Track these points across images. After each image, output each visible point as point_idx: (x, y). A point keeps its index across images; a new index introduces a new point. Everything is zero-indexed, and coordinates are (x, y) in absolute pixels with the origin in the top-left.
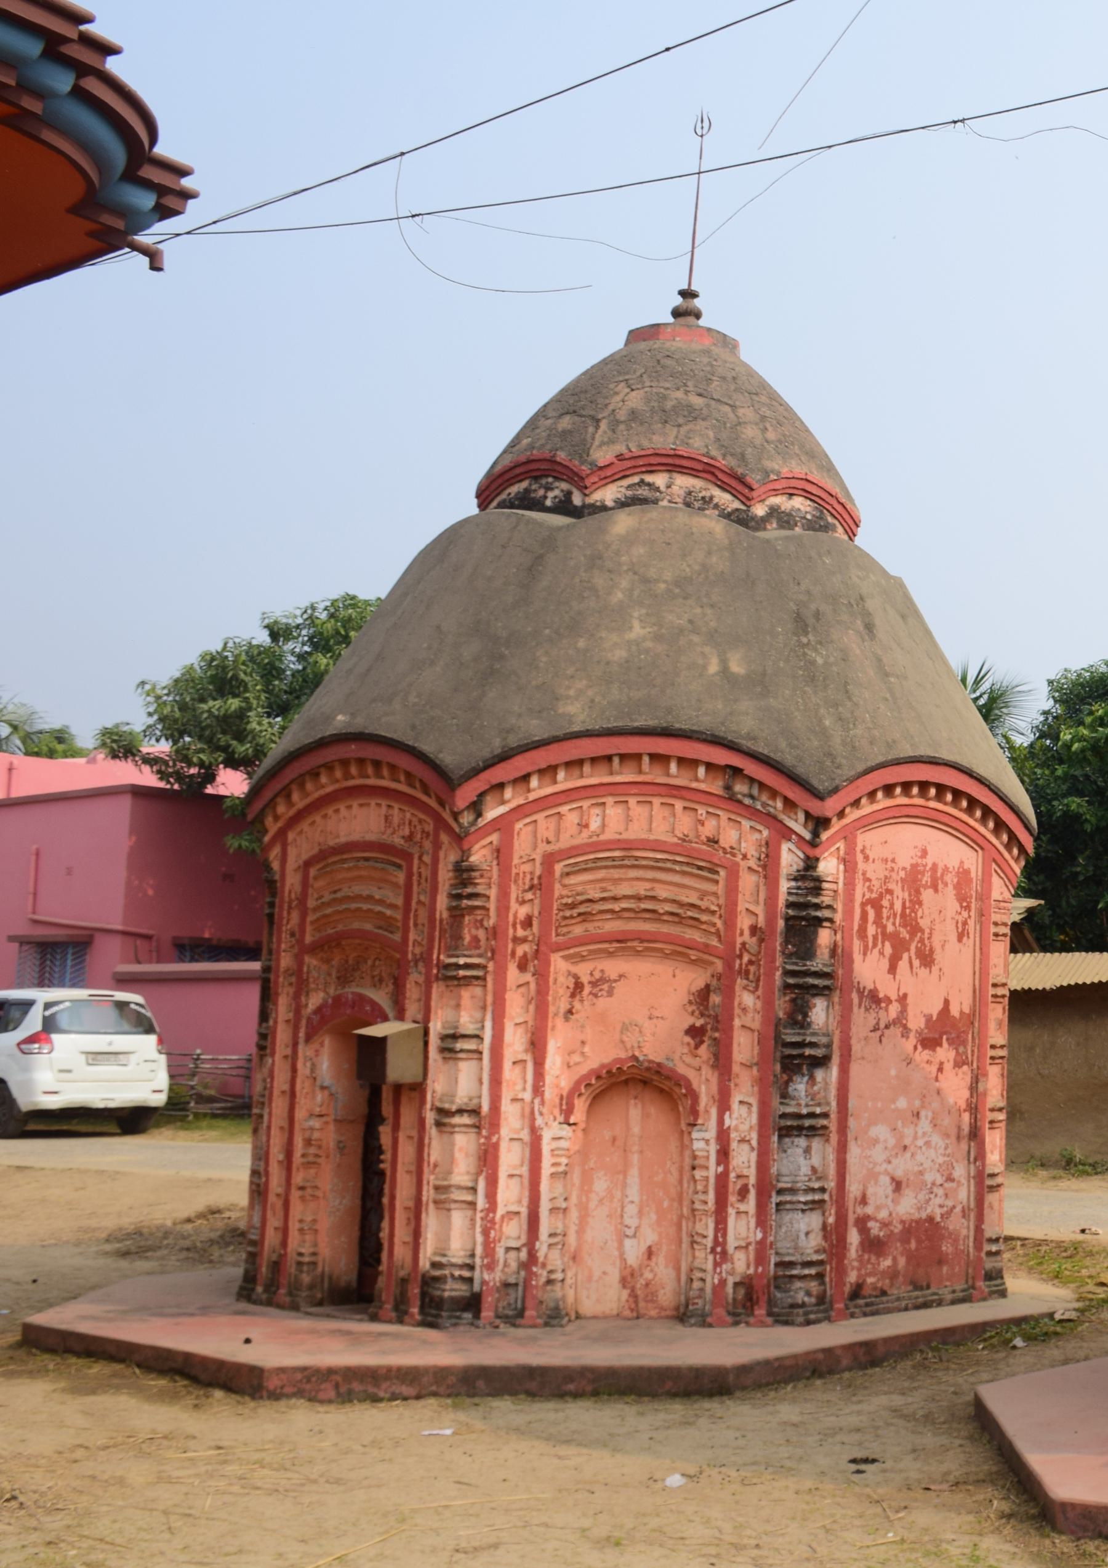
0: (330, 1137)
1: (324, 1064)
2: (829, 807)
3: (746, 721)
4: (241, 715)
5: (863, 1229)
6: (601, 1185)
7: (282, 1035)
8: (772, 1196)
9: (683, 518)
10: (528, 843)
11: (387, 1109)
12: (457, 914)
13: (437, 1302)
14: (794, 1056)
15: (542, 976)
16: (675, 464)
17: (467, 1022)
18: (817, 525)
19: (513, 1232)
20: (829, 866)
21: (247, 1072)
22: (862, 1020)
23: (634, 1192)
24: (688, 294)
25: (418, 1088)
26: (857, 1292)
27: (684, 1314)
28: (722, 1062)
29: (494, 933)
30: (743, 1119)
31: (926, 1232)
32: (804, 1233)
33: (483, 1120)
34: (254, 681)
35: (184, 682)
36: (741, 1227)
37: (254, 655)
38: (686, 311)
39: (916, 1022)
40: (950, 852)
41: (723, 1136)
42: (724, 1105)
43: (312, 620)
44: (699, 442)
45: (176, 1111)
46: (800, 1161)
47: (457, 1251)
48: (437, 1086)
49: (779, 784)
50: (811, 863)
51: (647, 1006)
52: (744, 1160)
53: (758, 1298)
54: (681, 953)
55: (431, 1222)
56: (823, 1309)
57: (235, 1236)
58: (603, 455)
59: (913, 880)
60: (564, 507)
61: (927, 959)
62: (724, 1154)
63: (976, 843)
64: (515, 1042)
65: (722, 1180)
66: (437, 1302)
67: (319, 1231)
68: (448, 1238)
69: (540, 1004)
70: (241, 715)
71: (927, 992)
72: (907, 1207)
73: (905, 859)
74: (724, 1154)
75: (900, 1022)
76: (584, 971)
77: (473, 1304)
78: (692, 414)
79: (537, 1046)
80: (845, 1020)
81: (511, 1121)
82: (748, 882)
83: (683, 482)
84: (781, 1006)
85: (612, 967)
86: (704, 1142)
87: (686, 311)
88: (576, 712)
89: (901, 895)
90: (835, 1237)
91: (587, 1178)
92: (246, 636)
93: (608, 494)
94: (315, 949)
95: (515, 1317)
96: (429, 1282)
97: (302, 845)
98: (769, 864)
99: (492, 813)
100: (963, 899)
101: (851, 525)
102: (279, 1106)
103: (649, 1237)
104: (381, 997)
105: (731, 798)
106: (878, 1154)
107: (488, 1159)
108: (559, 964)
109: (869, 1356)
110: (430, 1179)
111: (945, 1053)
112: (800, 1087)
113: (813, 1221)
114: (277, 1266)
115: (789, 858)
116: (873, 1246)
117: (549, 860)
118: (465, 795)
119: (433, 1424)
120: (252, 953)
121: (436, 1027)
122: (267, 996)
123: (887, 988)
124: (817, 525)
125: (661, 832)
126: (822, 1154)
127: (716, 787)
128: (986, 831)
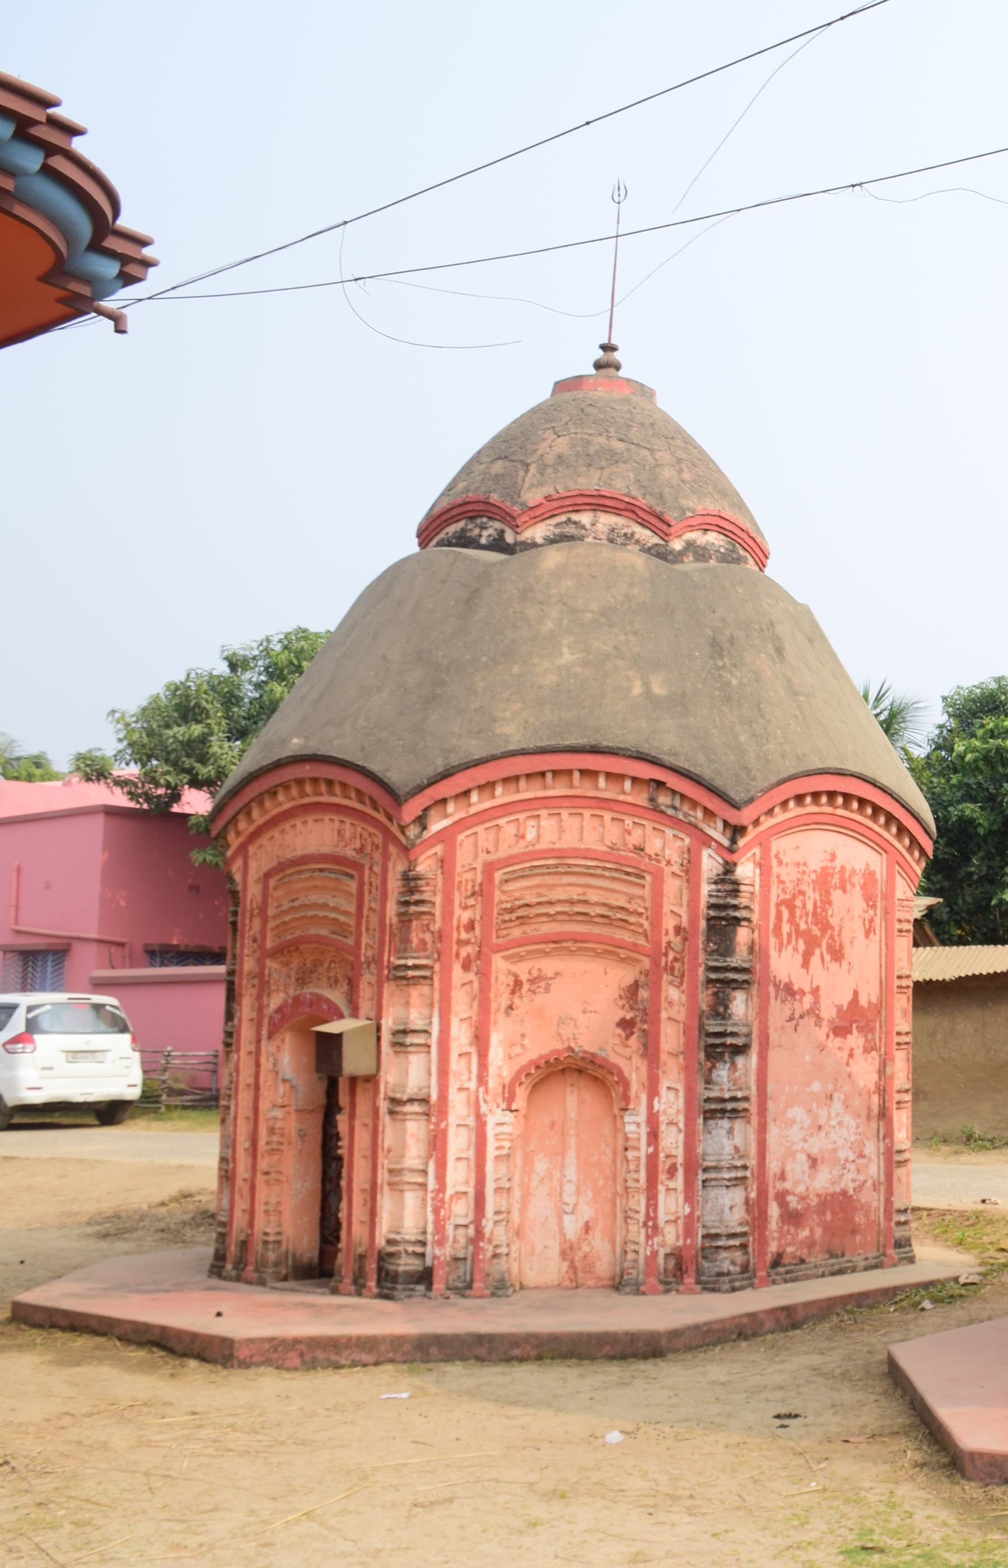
0: (292, 1125)
1: (286, 1060)
2: (744, 816)
3: (668, 739)
4: (203, 740)
5: (783, 1203)
6: (541, 1166)
7: (247, 1034)
8: (697, 1172)
9: (607, 553)
10: (470, 853)
11: (343, 1099)
12: (405, 919)
13: (391, 1277)
14: (718, 1047)
15: (484, 975)
16: (599, 503)
17: (416, 1019)
18: (729, 558)
19: (461, 1211)
20: (746, 871)
21: (214, 1067)
22: (778, 1011)
23: (571, 1172)
25: (372, 1080)
27: (618, 1284)
28: (650, 1051)
30: (671, 1103)
31: (840, 1205)
32: (728, 1208)
33: (433, 1108)
35: (151, 710)
36: (671, 1203)
39: (828, 1012)
40: (856, 856)
41: (653, 1119)
42: (653, 1090)
43: (267, 652)
44: (621, 483)
45: (150, 1103)
46: (723, 1141)
47: (410, 1228)
50: (729, 868)
51: (581, 1001)
52: (672, 1141)
53: (682, 1270)
54: (613, 952)
55: (386, 1202)
56: (747, 1277)
58: (532, 497)
59: (824, 881)
60: (498, 545)
61: (837, 954)
62: (654, 1136)
63: (881, 847)
64: (461, 1036)
65: (652, 1161)
66: (391, 1277)
67: (284, 1213)
68: (401, 1217)
70: (203, 740)
71: (836, 995)
72: (823, 1182)
73: (816, 863)
74: (654, 1136)
75: (813, 1012)
76: (522, 970)
78: (614, 458)
79: (481, 1039)
82: (672, 886)
83: (606, 520)
84: (704, 999)
85: (548, 966)
86: (635, 1124)
88: (512, 733)
89: (812, 896)
90: (756, 1211)
92: (207, 667)
93: (538, 532)
94: (277, 952)
95: (464, 1289)
96: (384, 1257)
97: (262, 858)
98: (691, 868)
99: (436, 826)
100: (869, 899)
101: (761, 557)
102: (245, 1098)
103: (587, 1213)
104: (337, 996)
105: (656, 809)
106: (795, 1134)
107: (437, 1143)
108: (499, 964)
109: (790, 1320)
111: (855, 1040)
112: (722, 1073)
113: (736, 1196)
114: (244, 1245)
115: (710, 863)
116: (792, 1218)
117: (489, 869)
118: (411, 810)
119: (392, 1388)
120: (217, 957)
121: (388, 1023)
122: (232, 996)
123: (801, 981)
124: (729, 558)
125: (591, 841)
127: (641, 799)
128: (890, 835)
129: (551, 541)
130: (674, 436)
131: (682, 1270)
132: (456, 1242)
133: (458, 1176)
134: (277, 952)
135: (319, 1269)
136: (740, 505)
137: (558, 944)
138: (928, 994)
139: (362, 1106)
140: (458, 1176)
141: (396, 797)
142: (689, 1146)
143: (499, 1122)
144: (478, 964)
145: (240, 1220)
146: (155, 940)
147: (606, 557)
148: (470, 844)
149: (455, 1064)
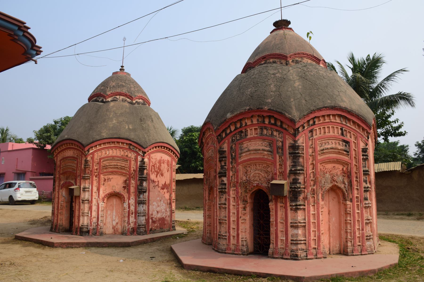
0: (65, 205)
1: (64, 193)
2: (146, 150)
3: (132, 136)
4: (50, 136)
6: (109, 212)
7: (57, 188)
9: (122, 103)
11: (74, 200)
12: (85, 168)
13: (82, 232)
14: (140, 191)
15: (99, 178)
16: (120, 94)
17: (87, 186)
19: (95, 220)
20: (146, 160)
21: (51, 194)
22: (152, 185)
23: (114, 214)
24: (122, 67)
25: (79, 197)
27: (123, 233)
28: (129, 192)
29: (91, 171)
30: (132, 201)
31: (162, 220)
32: (142, 220)
33: (90, 202)
34: (52, 130)
35: (41, 131)
36: (132, 219)
37: (52, 126)
39: (160, 185)
40: (166, 157)
41: (129, 204)
43: (61, 120)
44: (124, 91)
45: (40, 200)
46: (142, 208)
47: (85, 223)
48: (82, 196)
50: (143, 159)
51: (116, 183)
52: (132, 208)
53: (135, 231)
54: (122, 174)
55: (81, 218)
56: (145, 233)
57: (49, 221)
58: (108, 93)
59: (160, 162)
60: (102, 101)
61: (162, 175)
62: (129, 207)
63: (170, 156)
64: (95, 189)
65: (129, 211)
66: (82, 232)
67: (63, 220)
68: (84, 221)
70: (50, 136)
72: (159, 216)
73: (158, 159)
74: (129, 207)
75: (158, 185)
76: (106, 177)
78: (123, 86)
79: (98, 190)
81: (94, 202)
82: (133, 162)
83: (122, 97)
84: (138, 183)
85: (111, 177)
86: (126, 205)
88: (104, 135)
89: (158, 165)
90: (147, 221)
91: (107, 212)
93: (109, 99)
94: (62, 174)
95: (95, 234)
100: (168, 165)
102: (56, 200)
104: (73, 182)
105: (130, 149)
106: (154, 207)
107: (90, 208)
108: (102, 176)
109: (153, 240)
110: (81, 211)
111: (165, 190)
112: (141, 196)
114: (56, 226)
115: (139, 158)
116: (154, 222)
117: (100, 159)
118: (86, 149)
119: (82, 252)
120: (52, 175)
122: (54, 182)
123: (156, 180)
124: (144, 104)
125: (118, 154)
127: (127, 147)
129: (112, 101)
131: (135, 231)
132: (94, 225)
133: (94, 214)
134: (62, 174)
136: (146, 95)
137: (112, 173)
139: (77, 201)
140: (94, 214)
141: (83, 146)
142: (135, 209)
144: (98, 176)
145: (55, 221)
148: (98, 155)
149: (94, 194)
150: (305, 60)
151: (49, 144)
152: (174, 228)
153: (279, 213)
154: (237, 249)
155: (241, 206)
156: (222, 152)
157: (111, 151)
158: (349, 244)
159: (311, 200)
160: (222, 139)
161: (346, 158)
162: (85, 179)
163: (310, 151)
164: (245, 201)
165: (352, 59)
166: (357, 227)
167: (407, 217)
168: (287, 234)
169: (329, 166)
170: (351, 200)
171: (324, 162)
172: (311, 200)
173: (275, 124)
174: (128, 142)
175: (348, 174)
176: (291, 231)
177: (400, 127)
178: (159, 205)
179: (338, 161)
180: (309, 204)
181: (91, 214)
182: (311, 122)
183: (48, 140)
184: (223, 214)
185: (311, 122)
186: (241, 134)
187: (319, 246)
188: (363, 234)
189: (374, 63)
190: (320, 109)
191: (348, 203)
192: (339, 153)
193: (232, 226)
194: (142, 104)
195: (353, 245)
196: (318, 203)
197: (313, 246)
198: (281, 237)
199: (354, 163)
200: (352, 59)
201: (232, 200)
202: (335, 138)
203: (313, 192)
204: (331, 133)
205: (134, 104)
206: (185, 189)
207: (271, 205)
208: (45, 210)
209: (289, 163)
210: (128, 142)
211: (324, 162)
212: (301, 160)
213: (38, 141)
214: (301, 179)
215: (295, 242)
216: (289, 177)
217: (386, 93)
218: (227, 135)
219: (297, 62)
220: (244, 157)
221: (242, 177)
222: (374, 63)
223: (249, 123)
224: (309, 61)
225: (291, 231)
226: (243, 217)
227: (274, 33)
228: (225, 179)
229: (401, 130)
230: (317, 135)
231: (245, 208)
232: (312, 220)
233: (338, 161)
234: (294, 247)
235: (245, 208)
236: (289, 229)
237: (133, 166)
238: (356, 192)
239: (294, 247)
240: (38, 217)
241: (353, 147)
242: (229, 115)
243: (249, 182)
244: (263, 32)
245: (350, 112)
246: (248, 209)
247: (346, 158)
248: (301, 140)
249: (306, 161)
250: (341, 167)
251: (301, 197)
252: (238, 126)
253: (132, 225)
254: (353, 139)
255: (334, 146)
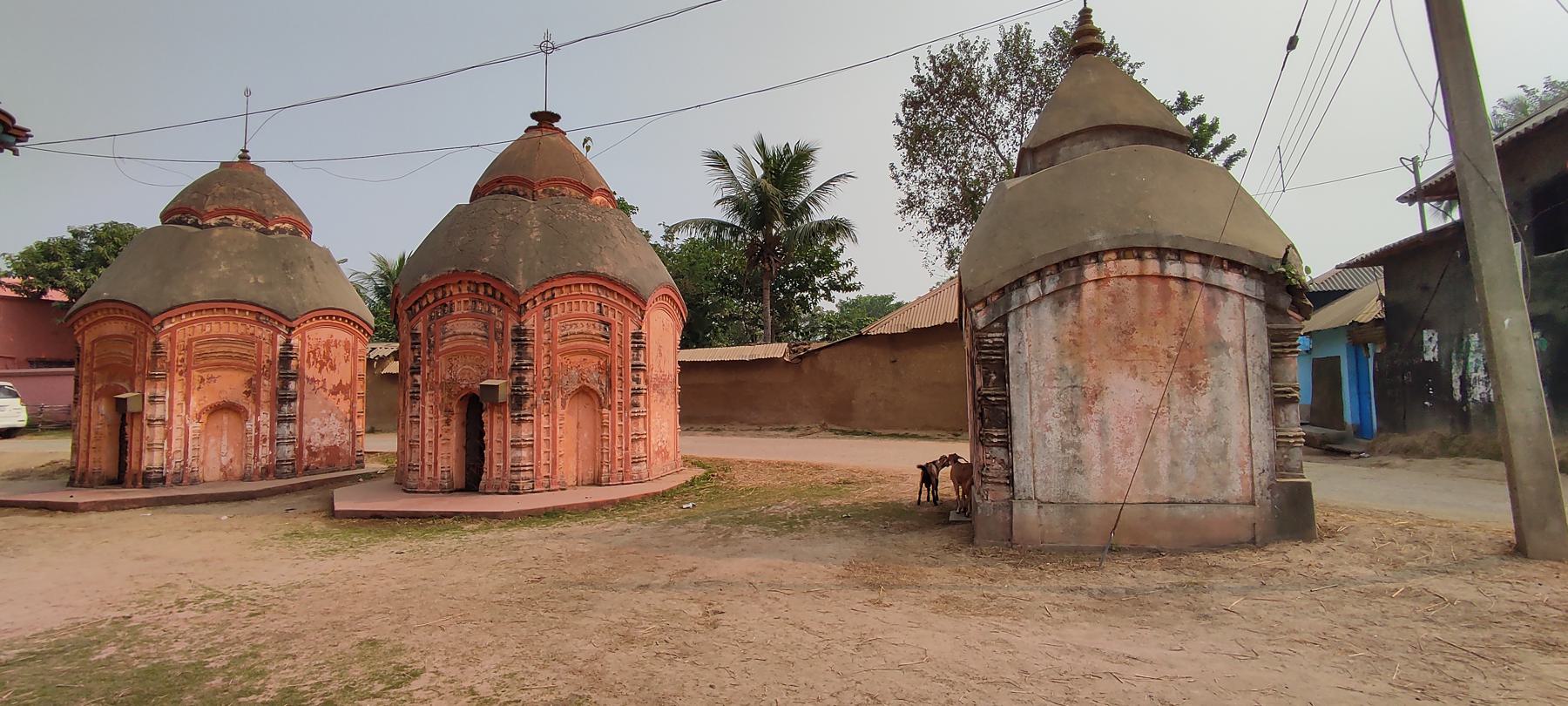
0: (106, 430)
1: (103, 407)
2: (294, 324)
3: (263, 298)
4: (60, 269)
5: (309, 448)
6: (212, 440)
7: (85, 399)
8: (275, 441)
9: (241, 232)
10: (182, 336)
11: (128, 420)
12: (155, 359)
13: (147, 480)
14: (282, 399)
15: (188, 377)
16: (238, 212)
17: (159, 392)
18: (295, 233)
19: (179, 457)
20: (295, 341)
21: (69, 411)
22: (308, 387)
23: (225, 442)
24: (245, 151)
25: (141, 414)
26: (307, 468)
27: (243, 479)
28: (257, 401)
29: (169, 364)
30: (264, 417)
31: (333, 450)
32: (288, 451)
33: (166, 423)
34: (64, 254)
35: (28, 253)
36: (264, 451)
37: (64, 243)
38: (244, 157)
39: (329, 387)
40: (341, 335)
41: (257, 424)
42: (257, 414)
43: (95, 231)
44: (248, 205)
45: (32, 428)
46: (285, 430)
47: (156, 464)
48: (148, 412)
49: (277, 317)
50: (288, 341)
51: (230, 385)
52: (265, 431)
53: (266, 473)
54: (241, 368)
55: (146, 456)
56: (294, 474)
57: (64, 469)
58: (210, 209)
59: (327, 344)
60: (195, 224)
61: (333, 368)
62: (258, 429)
63: (353, 333)
64: (178, 398)
65: (257, 437)
66: (147, 480)
67: (102, 459)
68: (153, 460)
69: (188, 385)
70: (60, 269)
71: (332, 379)
72: (326, 442)
73: (324, 339)
74: (258, 429)
75: (323, 387)
76: (204, 375)
77: (163, 480)
78: (245, 196)
79: (187, 399)
80: (302, 386)
81: (177, 422)
82: (265, 347)
83: (241, 219)
84: (278, 384)
85: (215, 374)
86: (250, 425)
87: (244, 157)
88: (199, 293)
89: (322, 349)
90: (299, 453)
91: (207, 440)
92: (59, 235)
93: (213, 222)
94: (98, 369)
95: (179, 483)
96: (145, 474)
97: (90, 336)
98: (273, 341)
99: (167, 326)
100: (347, 350)
101: (309, 234)
102: (84, 422)
103: (231, 456)
104: (125, 385)
105: (259, 321)
106: (315, 427)
107: (168, 435)
108: (195, 373)
109: (307, 486)
110: (145, 443)
111: (341, 396)
112: (285, 408)
113: (291, 447)
114: (83, 474)
115: (280, 339)
116: (313, 454)
117: (190, 341)
118: (156, 321)
119: (146, 514)
120: (70, 364)
121: (147, 394)
122: (77, 385)
123: (318, 377)
124: (295, 233)
125: (233, 331)
126: (293, 428)
127: (253, 318)
128: (355, 329)
129: (218, 225)
130: (273, 188)
131: (266, 473)
132: (176, 466)
133: (177, 445)
134: (98, 369)
135: (118, 481)
136: (300, 213)
137: (219, 366)
138: (686, 367)
139: (136, 422)
140: (177, 445)
141: (150, 317)
142: (271, 432)
143: (194, 427)
144: (186, 372)
145: (81, 465)
146: (33, 355)
147: (243, 233)
148: (180, 333)
149: (175, 407)
150: (566, 190)
151: (55, 287)
152: (360, 464)
153: (495, 427)
154: (433, 486)
155: (442, 419)
156: (415, 336)
157: (215, 326)
158: (605, 469)
159: (544, 408)
160: (415, 314)
161: (605, 347)
162: (152, 378)
163: (545, 337)
164: (449, 412)
165: (761, 147)
166: (618, 445)
167: (1399, 461)
168: (505, 458)
169: (577, 359)
170: (610, 408)
171: (564, 353)
172: (544, 408)
173: (493, 296)
174: (255, 309)
175: (607, 371)
176: (511, 454)
177: (851, 274)
178: (325, 423)
179: (591, 352)
180: (539, 414)
181: (170, 446)
182: (548, 295)
183: (54, 278)
184: (416, 431)
185: (548, 295)
186: (445, 307)
187: (554, 472)
188: (627, 456)
189: (801, 158)
190: (562, 277)
191: (605, 411)
192: (593, 340)
193: (427, 450)
194: (292, 233)
195: (610, 471)
196: (555, 412)
197: (544, 472)
198: (498, 462)
199: (617, 353)
200: (761, 147)
201: (427, 410)
202: (586, 317)
203: (547, 397)
204: (582, 311)
205: (272, 232)
206: (696, 378)
207: (485, 417)
208: (59, 448)
209: (511, 354)
210: (255, 309)
211: (564, 353)
212: (530, 350)
213: (18, 280)
214: (529, 377)
215: (517, 469)
216: (511, 375)
217: (818, 215)
218: (422, 308)
219: (552, 194)
220: (448, 344)
221: (444, 373)
222: (801, 158)
223: (456, 292)
224: (574, 192)
225: (511, 454)
226: (445, 435)
227: (531, 134)
228: (418, 377)
229: (853, 281)
230: (558, 311)
231: (448, 422)
232: (544, 436)
233: (591, 352)
234: (515, 476)
235: (448, 422)
236: (509, 449)
237: (267, 354)
238: (618, 395)
239: (515, 476)
240: (33, 464)
241: (618, 331)
242: (424, 279)
243: (454, 382)
244: (517, 125)
245: (611, 280)
246: (454, 423)
247: (605, 347)
248: (530, 322)
249: (538, 351)
250: (596, 360)
251: (528, 404)
252: (440, 295)
253: (264, 462)
254: (618, 319)
255: (585, 329)
